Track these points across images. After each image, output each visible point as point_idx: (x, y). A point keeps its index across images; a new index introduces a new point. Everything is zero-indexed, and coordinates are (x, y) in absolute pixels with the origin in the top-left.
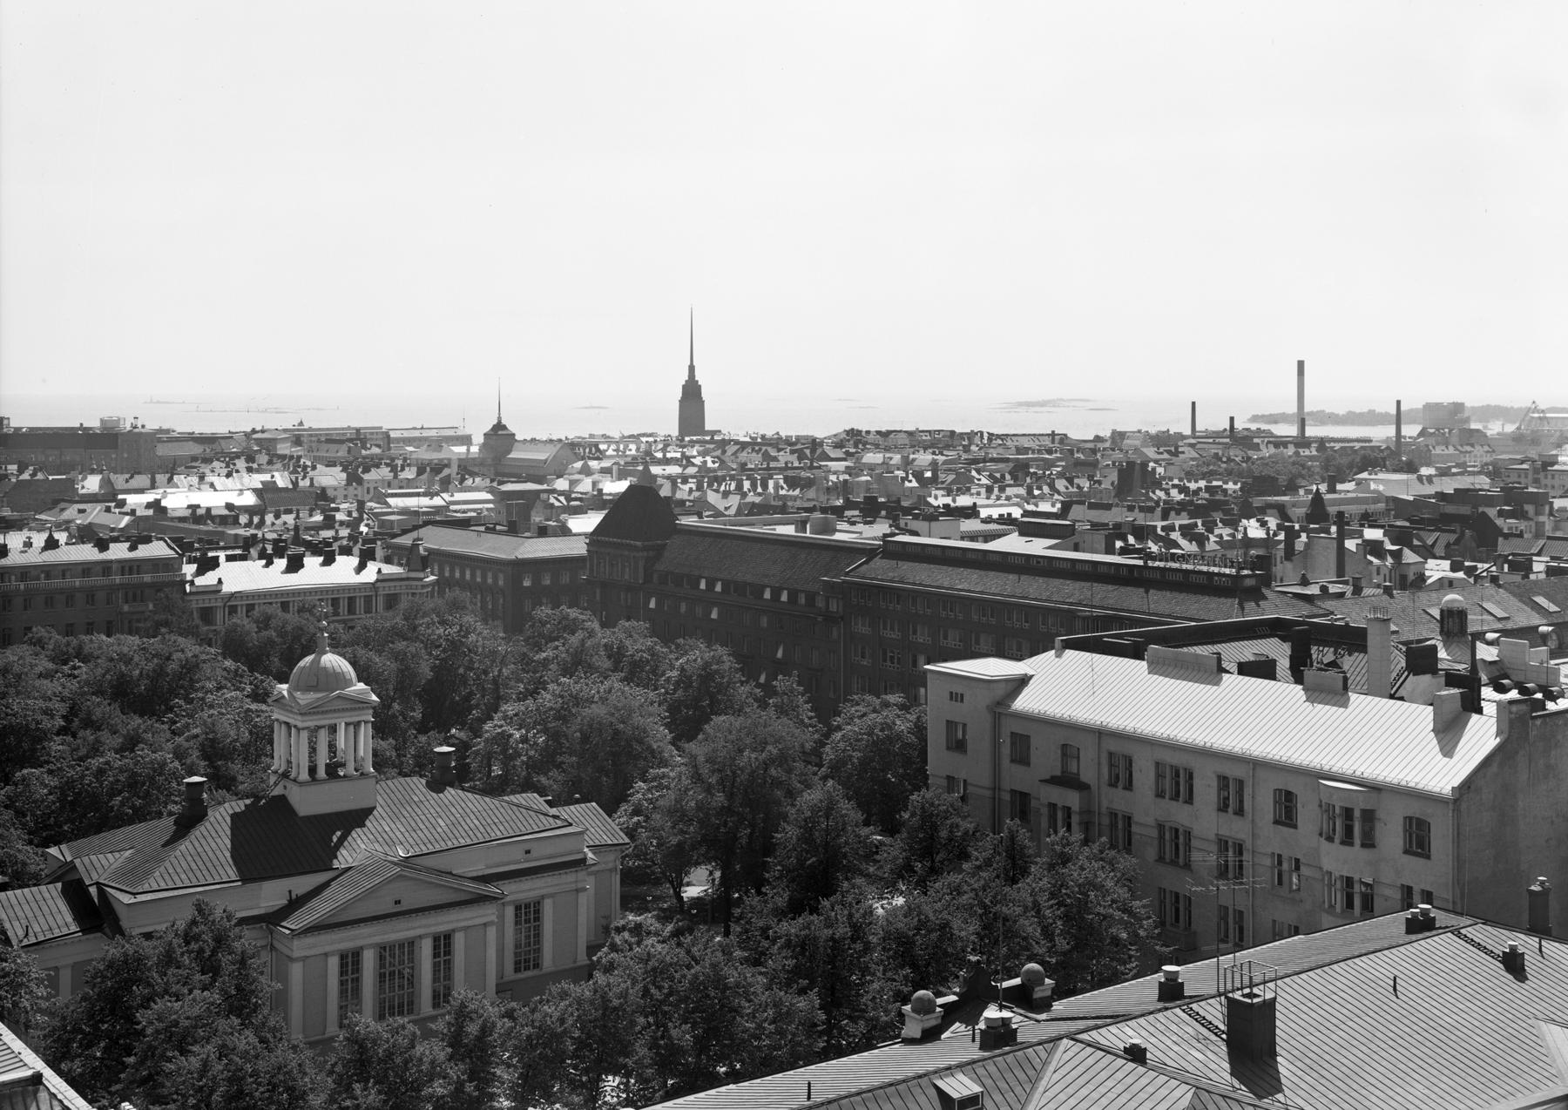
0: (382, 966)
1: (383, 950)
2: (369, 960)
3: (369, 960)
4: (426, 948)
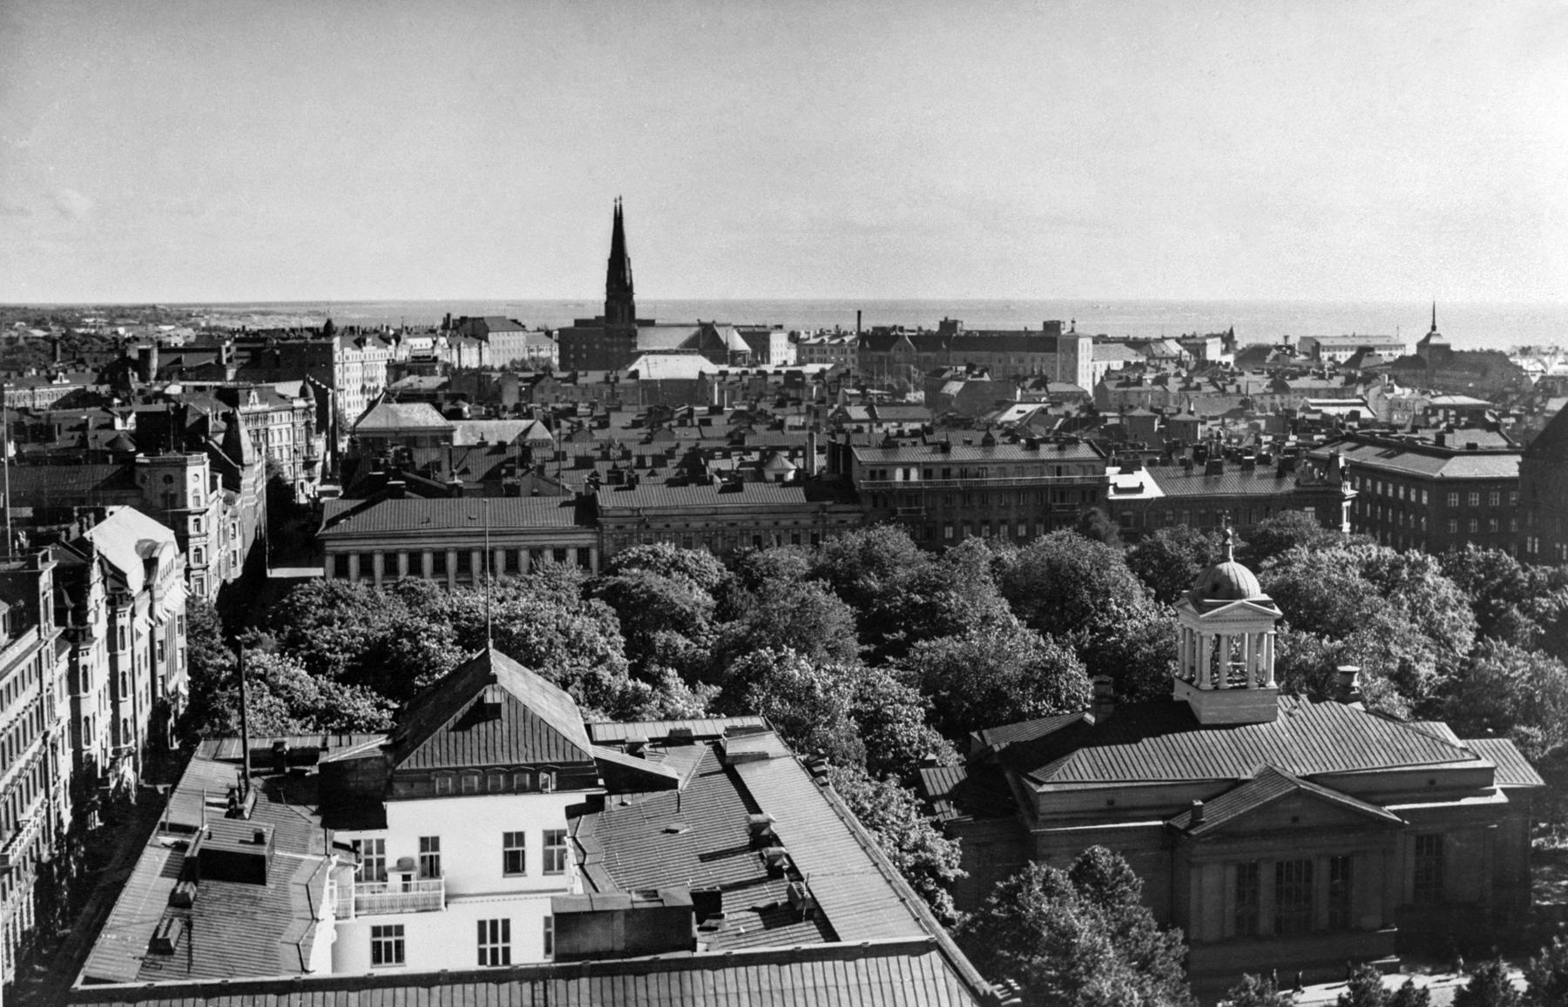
0: (1279, 882)
1: (1282, 870)
2: (1266, 875)
3: (1266, 875)
4: (1322, 869)
